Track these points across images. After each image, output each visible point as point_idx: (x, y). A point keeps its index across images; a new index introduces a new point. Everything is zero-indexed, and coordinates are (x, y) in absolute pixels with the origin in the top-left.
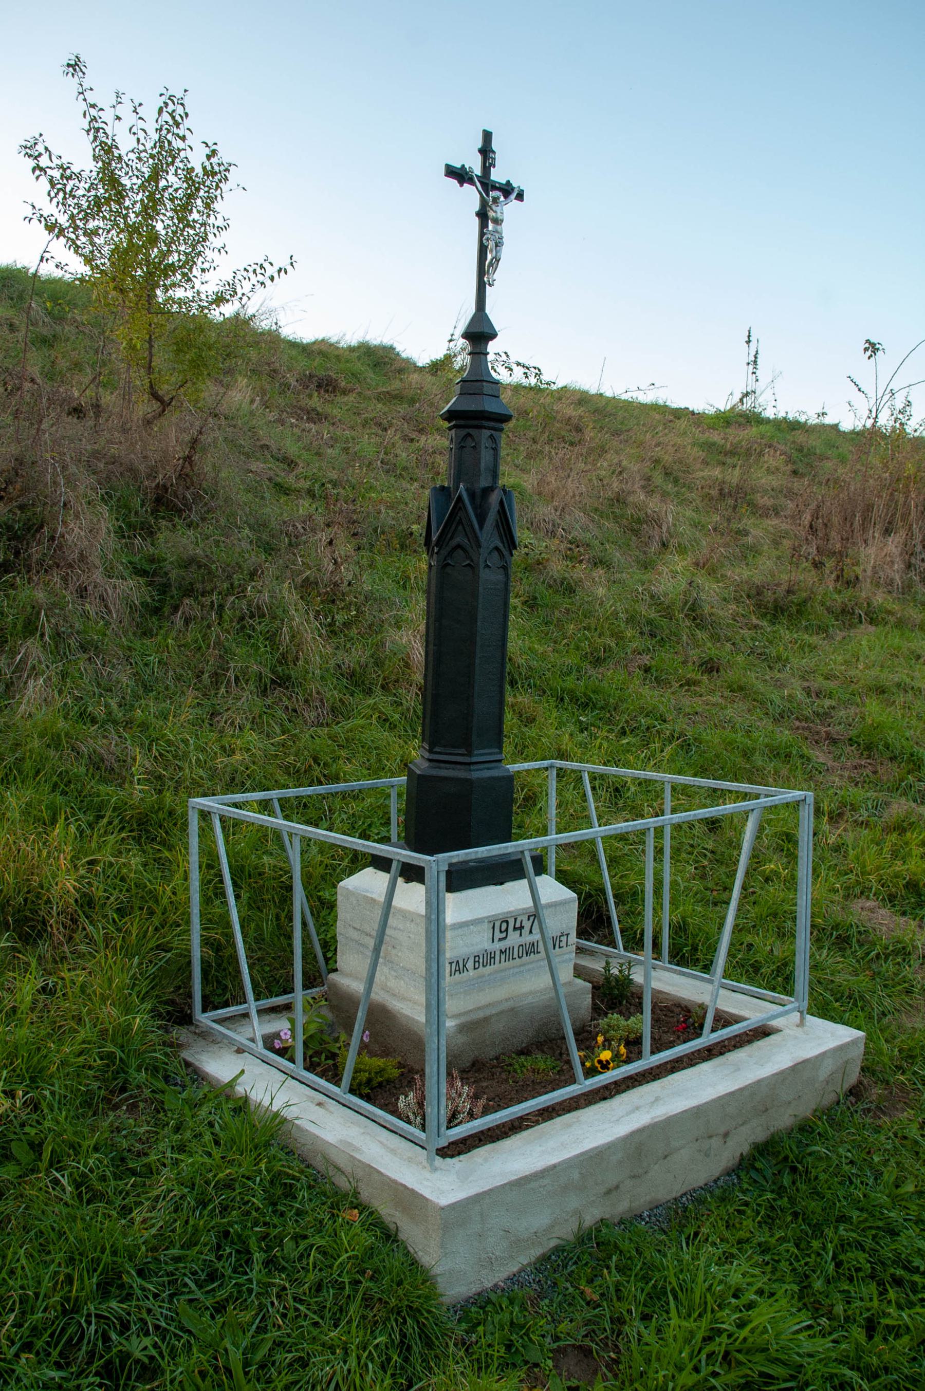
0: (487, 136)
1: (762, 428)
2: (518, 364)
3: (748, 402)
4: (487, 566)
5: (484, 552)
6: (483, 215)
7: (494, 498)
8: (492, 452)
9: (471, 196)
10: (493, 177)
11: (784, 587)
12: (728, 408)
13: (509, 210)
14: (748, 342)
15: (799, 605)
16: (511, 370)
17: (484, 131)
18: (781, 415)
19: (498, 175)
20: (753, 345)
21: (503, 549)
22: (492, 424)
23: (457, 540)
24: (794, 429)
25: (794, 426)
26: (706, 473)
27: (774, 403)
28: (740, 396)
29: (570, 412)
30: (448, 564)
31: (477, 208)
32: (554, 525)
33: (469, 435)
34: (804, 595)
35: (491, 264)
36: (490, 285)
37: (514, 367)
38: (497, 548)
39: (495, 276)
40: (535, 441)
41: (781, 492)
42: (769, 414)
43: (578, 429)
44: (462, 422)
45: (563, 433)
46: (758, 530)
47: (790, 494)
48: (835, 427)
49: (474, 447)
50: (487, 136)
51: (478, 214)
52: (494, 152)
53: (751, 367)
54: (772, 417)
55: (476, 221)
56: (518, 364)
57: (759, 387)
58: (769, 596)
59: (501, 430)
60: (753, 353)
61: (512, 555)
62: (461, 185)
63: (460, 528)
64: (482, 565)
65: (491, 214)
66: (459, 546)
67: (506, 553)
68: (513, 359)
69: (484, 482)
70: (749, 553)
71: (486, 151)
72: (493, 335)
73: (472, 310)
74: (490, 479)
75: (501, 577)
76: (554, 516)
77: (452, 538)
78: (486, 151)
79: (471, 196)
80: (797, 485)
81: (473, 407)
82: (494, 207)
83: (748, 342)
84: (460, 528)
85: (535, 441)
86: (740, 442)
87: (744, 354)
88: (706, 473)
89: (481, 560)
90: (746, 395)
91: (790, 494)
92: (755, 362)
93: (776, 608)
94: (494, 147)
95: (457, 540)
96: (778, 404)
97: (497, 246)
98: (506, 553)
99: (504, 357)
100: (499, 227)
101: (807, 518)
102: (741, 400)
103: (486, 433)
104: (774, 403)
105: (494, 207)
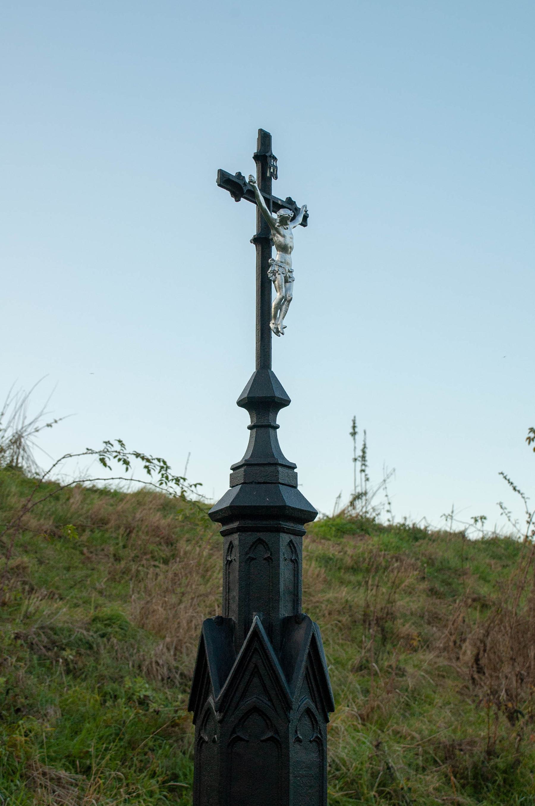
0: (265, 139)
1: (385, 538)
2: (137, 455)
3: (359, 504)
4: (298, 740)
5: (294, 715)
6: (263, 241)
7: (300, 635)
8: (291, 566)
9: (247, 213)
10: (274, 193)
11: (479, 749)
12: (338, 512)
13: (294, 234)
14: (354, 434)
15: (505, 772)
16: (126, 462)
17: (261, 131)
18: (398, 520)
19: (279, 190)
20: (360, 437)
21: (316, 712)
22: (290, 525)
23: (251, 700)
24: (416, 539)
25: (416, 535)
26: (330, 595)
27: (387, 507)
28: (350, 498)
29: (156, 518)
30: (240, 739)
31: (253, 231)
32: (169, 669)
33: (260, 541)
34: (511, 758)
35: (279, 306)
36: (277, 333)
37: (132, 459)
38: (308, 711)
39: (285, 322)
40: (117, 559)
41: (422, 617)
42: (383, 520)
43: (170, 543)
44: (249, 523)
45: (151, 547)
46: (417, 667)
47: (434, 619)
48: (462, 535)
49: (269, 559)
50: (265, 139)
51: (256, 240)
52: (275, 159)
53: (359, 464)
54: (386, 524)
55: (252, 250)
56: (137, 455)
57: (371, 487)
58: (466, 761)
59: (302, 534)
60: (360, 447)
61: (327, 721)
62: (238, 200)
63: (256, 680)
64: (292, 739)
65: (278, 238)
66: (255, 709)
67: (319, 718)
68: (130, 449)
69: (284, 611)
70: (414, 701)
71: (264, 158)
72: (285, 402)
73: (250, 368)
74: (290, 605)
75: (314, 756)
76: (169, 656)
77: (243, 696)
78: (264, 158)
79: (247, 213)
80: (442, 608)
81: (267, 501)
82: (281, 230)
83: (354, 434)
84: (256, 680)
85: (117, 559)
86: (363, 553)
87: (349, 449)
88: (330, 595)
89: (291, 730)
90: (358, 497)
91: (434, 619)
92: (363, 457)
93: (475, 777)
94: (275, 151)
95: (251, 700)
96: (393, 508)
97: (286, 281)
98: (319, 718)
99: (117, 447)
100: (287, 256)
101: (468, 651)
102: (352, 504)
103: (285, 538)
104: (387, 507)
105: (281, 230)
